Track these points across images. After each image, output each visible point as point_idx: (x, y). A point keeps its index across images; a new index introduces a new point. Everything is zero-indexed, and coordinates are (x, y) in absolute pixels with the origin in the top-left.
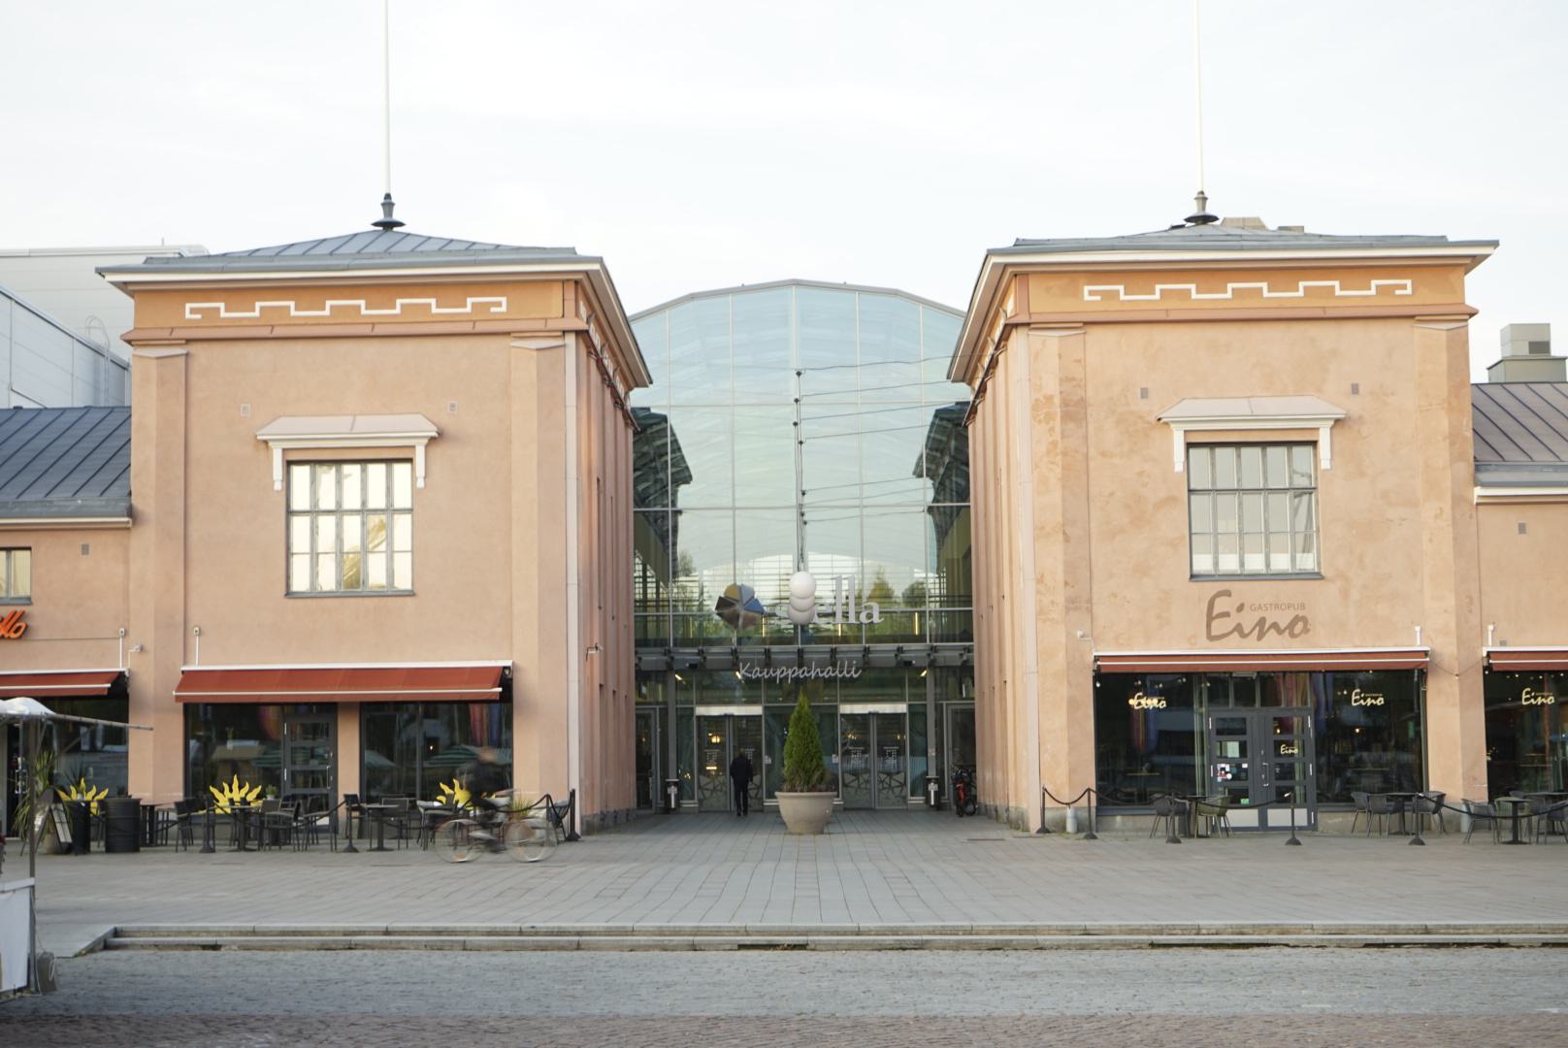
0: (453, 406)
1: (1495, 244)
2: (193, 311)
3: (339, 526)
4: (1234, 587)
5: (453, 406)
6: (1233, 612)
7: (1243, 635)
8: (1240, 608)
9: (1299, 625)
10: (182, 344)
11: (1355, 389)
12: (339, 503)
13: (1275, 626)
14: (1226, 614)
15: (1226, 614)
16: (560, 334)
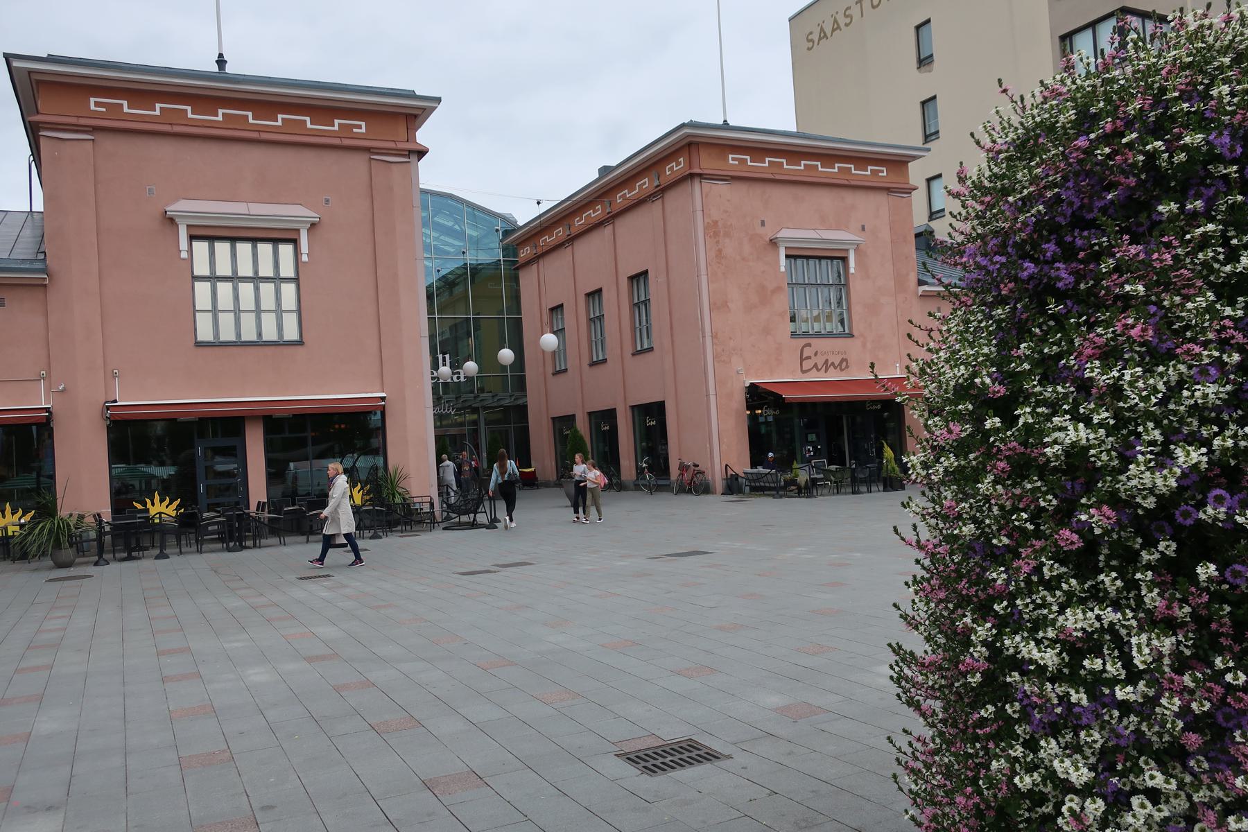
0: (327, 201)
1: (438, 100)
2: (733, 159)
3: (236, 290)
4: (813, 341)
5: (327, 201)
6: (813, 356)
7: (818, 370)
8: (816, 354)
9: (843, 364)
10: (90, 131)
11: (863, 228)
12: (235, 270)
13: (833, 364)
14: (809, 358)
15: (809, 358)
16: (407, 153)
